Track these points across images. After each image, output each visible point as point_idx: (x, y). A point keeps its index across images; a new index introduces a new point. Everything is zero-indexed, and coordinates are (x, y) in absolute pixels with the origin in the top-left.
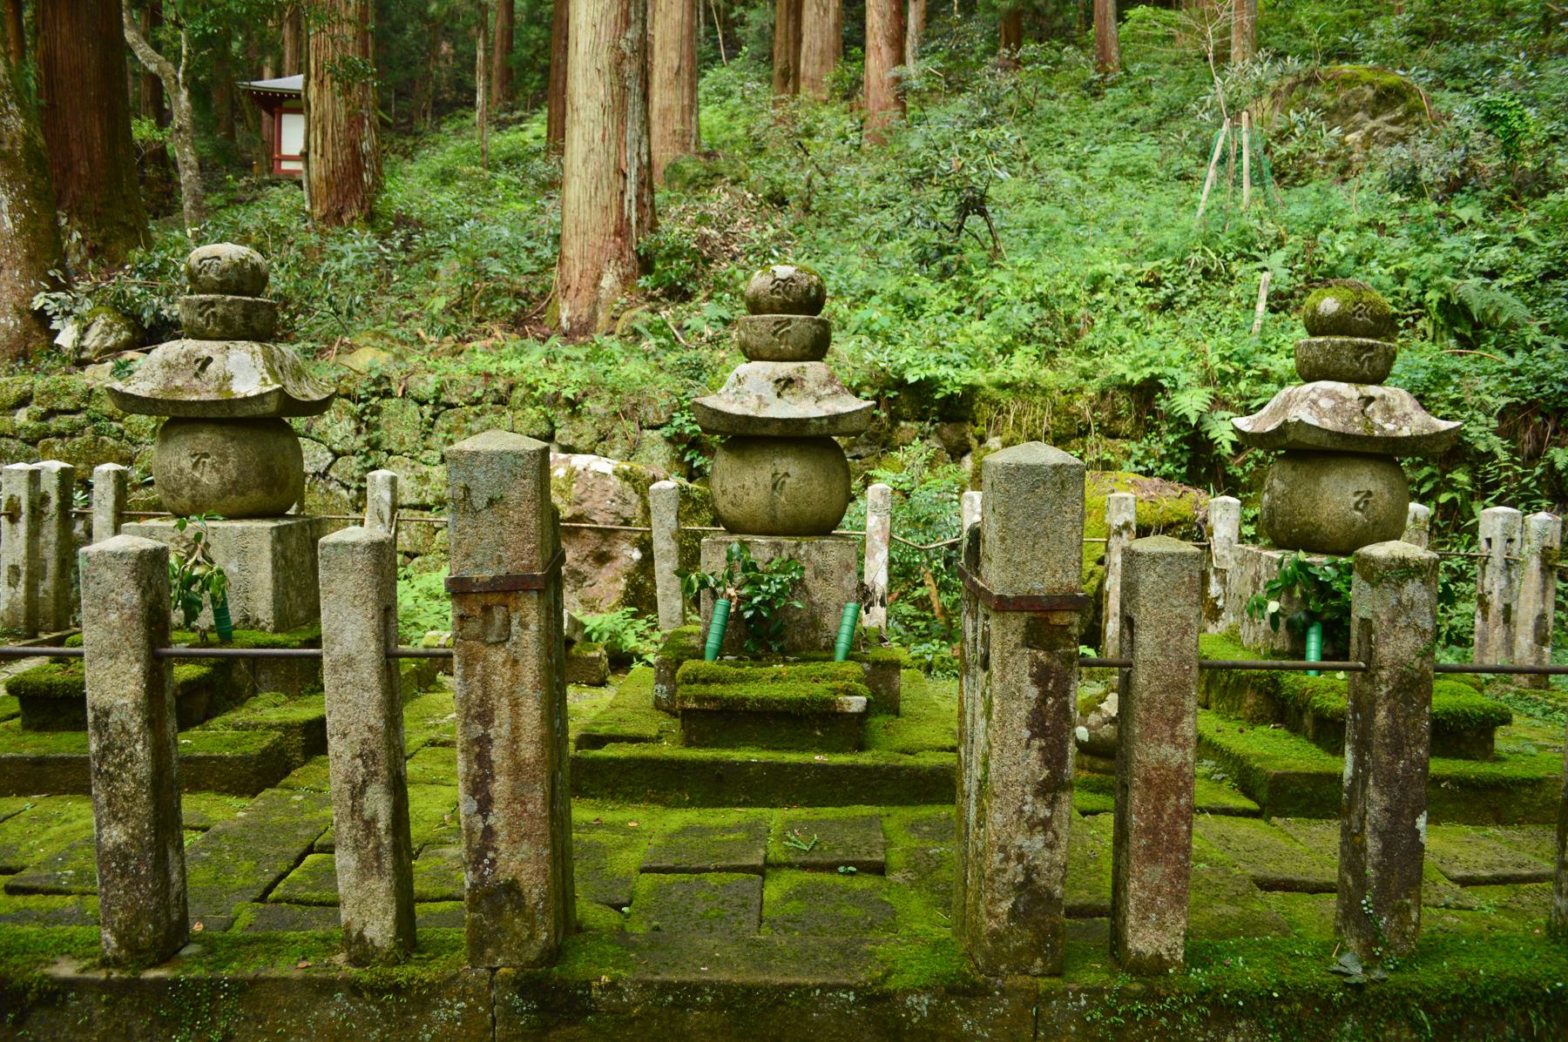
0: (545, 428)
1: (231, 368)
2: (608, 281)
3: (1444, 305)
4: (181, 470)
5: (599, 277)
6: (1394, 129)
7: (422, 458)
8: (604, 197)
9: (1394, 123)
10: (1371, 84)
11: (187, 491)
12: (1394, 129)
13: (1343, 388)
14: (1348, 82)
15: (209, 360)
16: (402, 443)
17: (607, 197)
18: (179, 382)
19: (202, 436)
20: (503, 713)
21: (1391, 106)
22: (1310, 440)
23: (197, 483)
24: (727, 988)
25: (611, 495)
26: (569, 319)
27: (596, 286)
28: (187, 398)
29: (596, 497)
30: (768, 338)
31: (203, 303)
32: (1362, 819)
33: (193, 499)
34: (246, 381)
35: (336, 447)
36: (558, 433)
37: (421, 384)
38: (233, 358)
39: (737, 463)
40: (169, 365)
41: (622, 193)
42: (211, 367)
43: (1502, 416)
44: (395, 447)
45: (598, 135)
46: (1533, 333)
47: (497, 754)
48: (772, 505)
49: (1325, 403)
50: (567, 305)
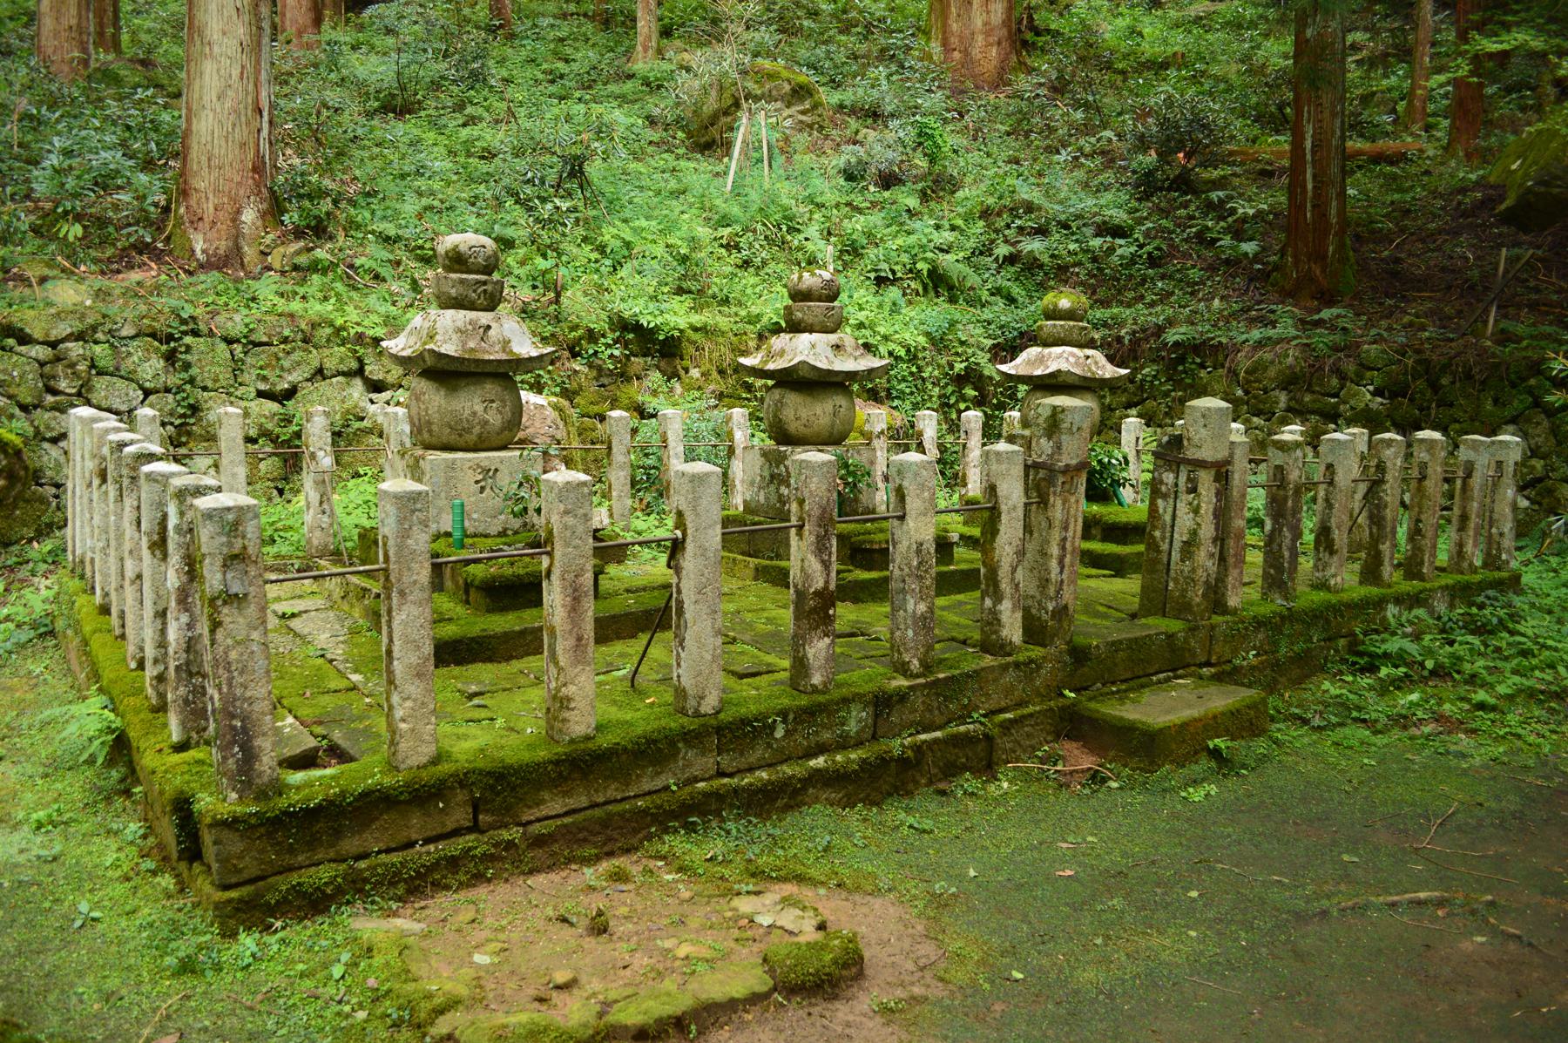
0: (354, 365)
1: (507, 334)
2: (249, 216)
3: (933, 273)
4: (474, 414)
5: (239, 212)
6: (804, 118)
7: (238, 393)
8: (241, 134)
9: (803, 113)
10: (789, 81)
11: (477, 430)
12: (804, 118)
13: (1075, 350)
14: (771, 76)
15: (489, 327)
16: (216, 381)
17: (245, 133)
18: (472, 345)
19: (488, 386)
20: (1072, 527)
21: (801, 100)
22: (1070, 380)
23: (487, 422)
24: (1130, 640)
25: (549, 422)
26: (203, 251)
27: (234, 220)
28: (487, 357)
29: (537, 424)
30: (821, 318)
31: (478, 282)
32: (1280, 546)
33: (480, 436)
34: (521, 344)
35: (147, 385)
36: (368, 369)
37: (230, 324)
38: (506, 326)
39: (809, 400)
40: (459, 331)
41: (259, 131)
42: (491, 332)
43: (990, 351)
44: (210, 384)
45: (236, 73)
46: (985, 295)
47: (1068, 545)
48: (833, 426)
49: (1072, 360)
50: (200, 237)
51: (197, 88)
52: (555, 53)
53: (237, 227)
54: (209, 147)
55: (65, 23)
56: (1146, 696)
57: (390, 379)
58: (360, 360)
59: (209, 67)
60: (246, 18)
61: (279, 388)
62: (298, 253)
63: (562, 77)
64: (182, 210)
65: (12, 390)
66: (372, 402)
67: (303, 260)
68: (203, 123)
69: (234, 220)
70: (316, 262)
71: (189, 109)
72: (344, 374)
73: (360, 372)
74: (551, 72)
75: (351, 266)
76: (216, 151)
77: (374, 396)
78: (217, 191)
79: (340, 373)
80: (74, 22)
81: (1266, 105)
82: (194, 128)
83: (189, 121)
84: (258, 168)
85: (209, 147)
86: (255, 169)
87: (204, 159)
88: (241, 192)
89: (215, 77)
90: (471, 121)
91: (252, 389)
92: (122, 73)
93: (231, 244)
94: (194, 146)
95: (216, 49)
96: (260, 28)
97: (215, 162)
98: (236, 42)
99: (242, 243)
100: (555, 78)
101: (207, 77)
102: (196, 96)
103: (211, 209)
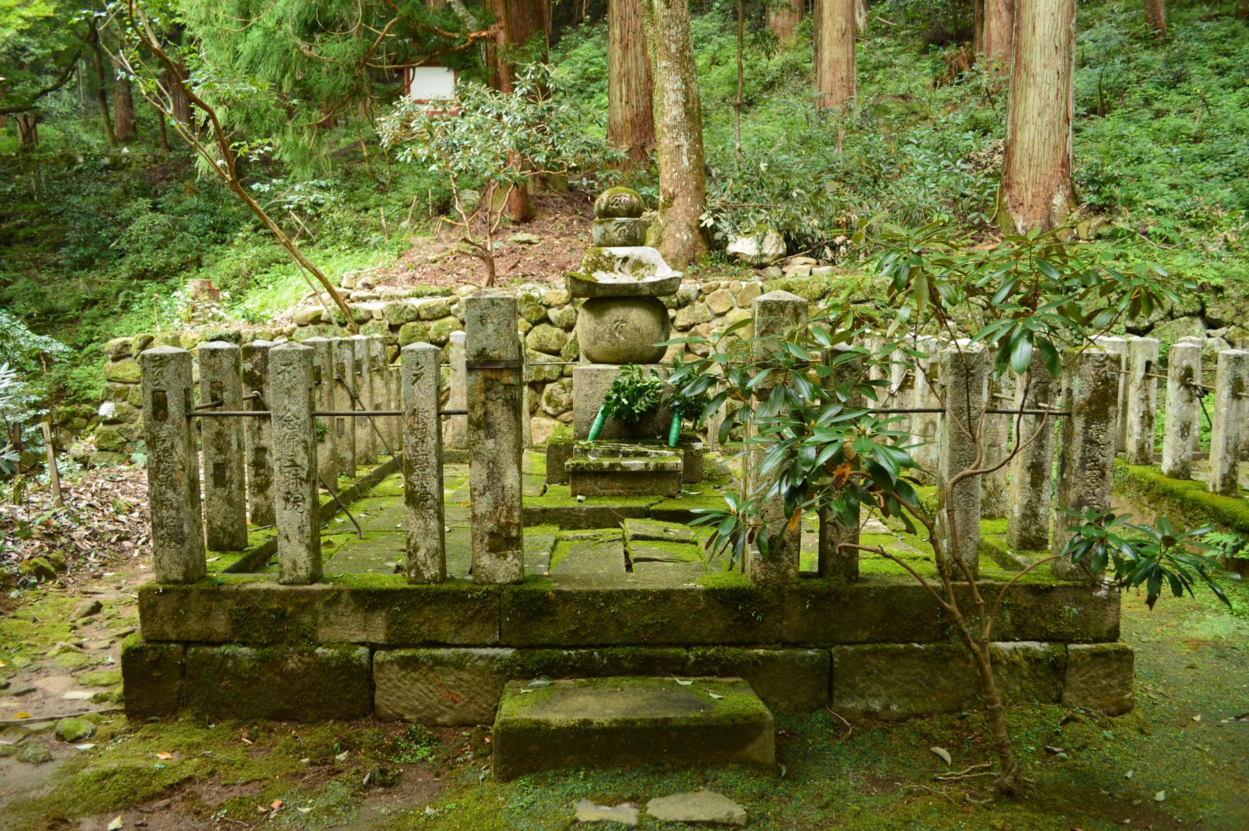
0: (1198, 308)
2: (1059, 200)
5: (1051, 197)
36: (1209, 311)
45: (1053, 95)
50: (1021, 218)
51: (1022, 109)
52: (1216, 50)
53: (1049, 209)
54: (1030, 151)
55: (839, 76)
56: (749, 711)
57: (1226, 318)
58: (1203, 305)
59: (1032, 93)
60: (1062, 53)
61: (1142, 325)
62: (1099, 225)
63: (1230, 68)
64: (1006, 199)
65: (967, 327)
66: (1209, 336)
67: (1105, 230)
68: (1026, 134)
69: (1046, 204)
70: (1116, 231)
71: (1014, 124)
72: (1189, 315)
73: (1201, 313)
74: (1218, 67)
75: (1145, 234)
76: (1036, 153)
77: (1211, 332)
78: (1035, 183)
79: (1186, 314)
80: (844, 74)
81: (323, 41)
82: (1018, 138)
83: (1014, 133)
84: (1065, 164)
85: (1030, 151)
86: (1063, 165)
87: (1025, 160)
88: (1053, 183)
89: (1037, 100)
90: (1159, 114)
91: (1122, 326)
92: (890, 106)
93: (1044, 221)
94: (1018, 152)
95: (1039, 79)
96: (1070, 59)
97: (1034, 162)
98: (1054, 72)
99: (1053, 220)
100: (1222, 71)
101: (1031, 100)
102: (1021, 115)
103: (1030, 197)
